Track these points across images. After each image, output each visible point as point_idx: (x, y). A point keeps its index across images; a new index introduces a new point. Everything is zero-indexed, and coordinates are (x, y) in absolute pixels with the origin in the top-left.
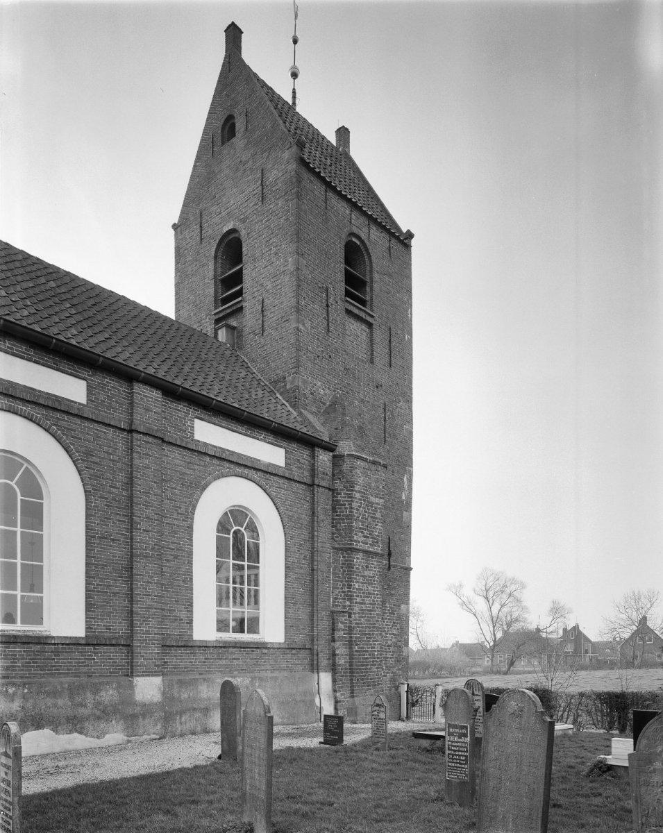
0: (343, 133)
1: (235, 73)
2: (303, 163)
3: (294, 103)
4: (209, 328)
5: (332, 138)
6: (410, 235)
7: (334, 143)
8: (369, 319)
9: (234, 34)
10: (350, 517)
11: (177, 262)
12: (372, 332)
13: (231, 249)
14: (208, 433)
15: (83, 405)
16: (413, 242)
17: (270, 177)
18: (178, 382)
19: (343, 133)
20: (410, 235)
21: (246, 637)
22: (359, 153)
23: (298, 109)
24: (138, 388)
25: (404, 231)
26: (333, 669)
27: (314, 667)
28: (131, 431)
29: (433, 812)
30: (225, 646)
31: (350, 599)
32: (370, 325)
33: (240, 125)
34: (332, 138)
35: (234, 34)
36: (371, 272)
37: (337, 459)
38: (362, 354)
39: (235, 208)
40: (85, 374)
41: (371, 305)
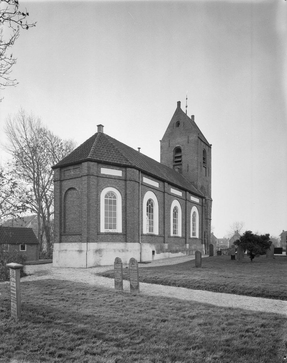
0: (193, 116)
1: (179, 111)
2: (199, 137)
3: (186, 113)
4: (172, 167)
5: (191, 118)
6: (211, 145)
7: (191, 118)
8: (206, 167)
9: (179, 103)
10: (207, 212)
11: (161, 149)
12: (206, 169)
13: (178, 150)
14: (147, 180)
15: (102, 167)
16: (212, 147)
17: (191, 139)
18: (153, 173)
19: (193, 116)
20: (211, 145)
21: (111, 231)
22: (196, 121)
23: (187, 115)
24: (128, 169)
25: (210, 144)
26: (205, 244)
27: (202, 243)
28: (126, 180)
29: (103, 306)
30: (106, 234)
31: (207, 229)
32: (206, 168)
33: (181, 124)
34: (191, 118)
35: (179, 103)
36: (206, 156)
37: (206, 200)
38: (204, 175)
39: (179, 141)
40: (159, 181)
41: (206, 163)
